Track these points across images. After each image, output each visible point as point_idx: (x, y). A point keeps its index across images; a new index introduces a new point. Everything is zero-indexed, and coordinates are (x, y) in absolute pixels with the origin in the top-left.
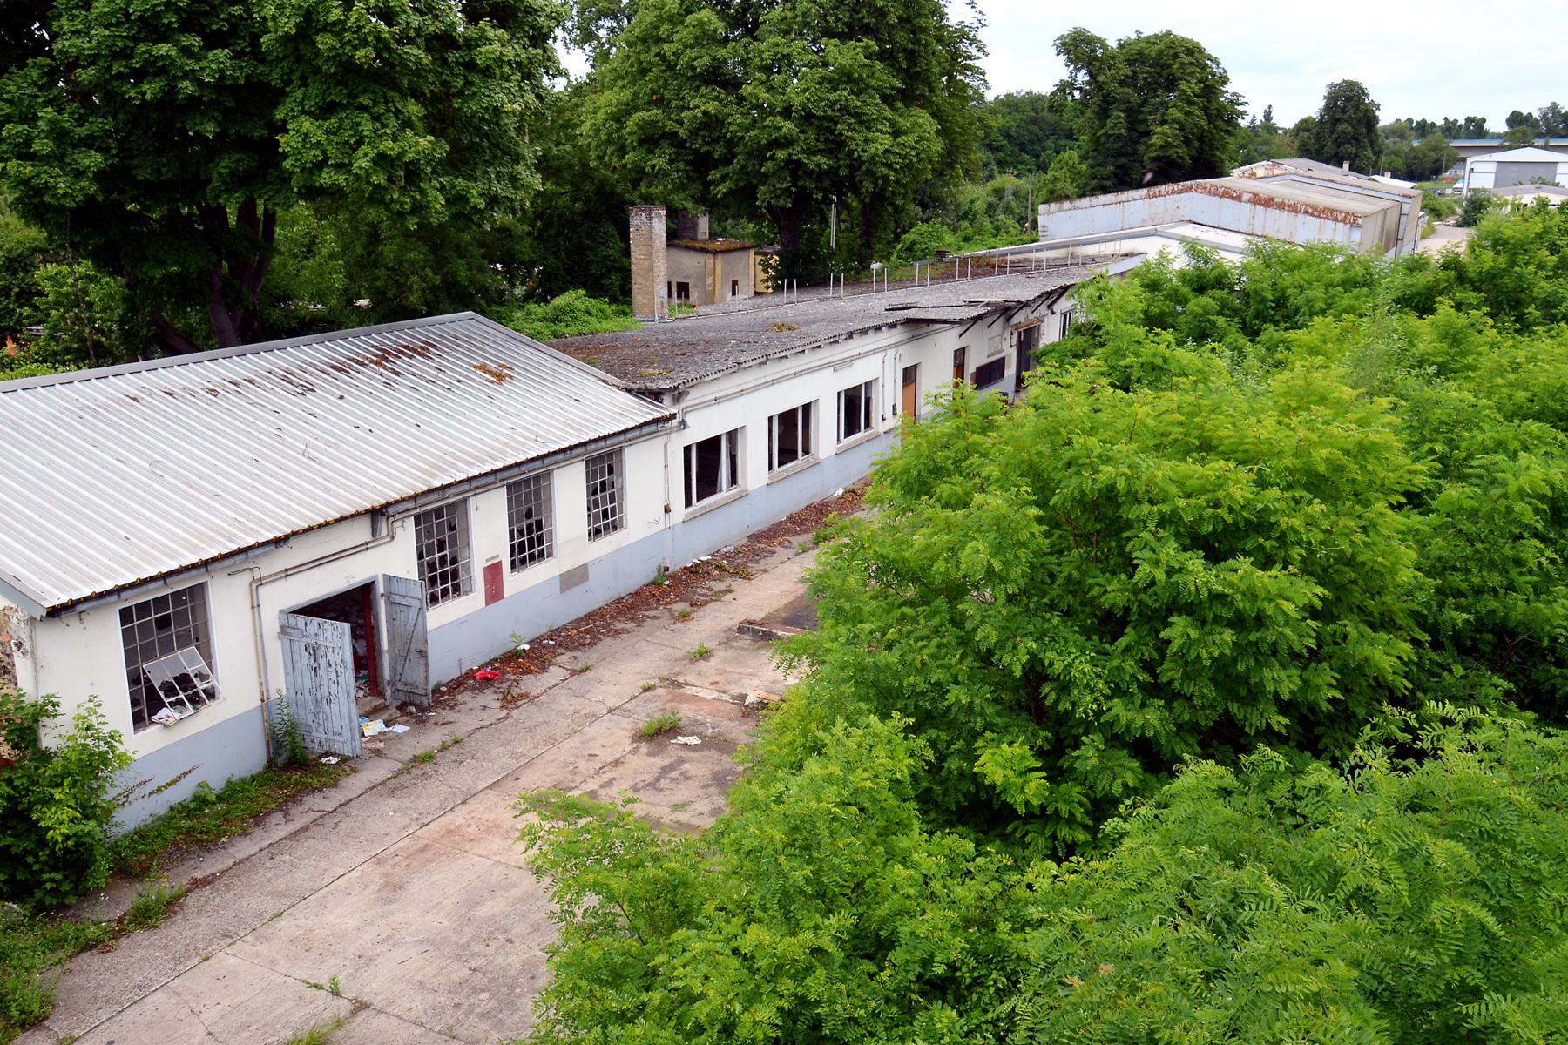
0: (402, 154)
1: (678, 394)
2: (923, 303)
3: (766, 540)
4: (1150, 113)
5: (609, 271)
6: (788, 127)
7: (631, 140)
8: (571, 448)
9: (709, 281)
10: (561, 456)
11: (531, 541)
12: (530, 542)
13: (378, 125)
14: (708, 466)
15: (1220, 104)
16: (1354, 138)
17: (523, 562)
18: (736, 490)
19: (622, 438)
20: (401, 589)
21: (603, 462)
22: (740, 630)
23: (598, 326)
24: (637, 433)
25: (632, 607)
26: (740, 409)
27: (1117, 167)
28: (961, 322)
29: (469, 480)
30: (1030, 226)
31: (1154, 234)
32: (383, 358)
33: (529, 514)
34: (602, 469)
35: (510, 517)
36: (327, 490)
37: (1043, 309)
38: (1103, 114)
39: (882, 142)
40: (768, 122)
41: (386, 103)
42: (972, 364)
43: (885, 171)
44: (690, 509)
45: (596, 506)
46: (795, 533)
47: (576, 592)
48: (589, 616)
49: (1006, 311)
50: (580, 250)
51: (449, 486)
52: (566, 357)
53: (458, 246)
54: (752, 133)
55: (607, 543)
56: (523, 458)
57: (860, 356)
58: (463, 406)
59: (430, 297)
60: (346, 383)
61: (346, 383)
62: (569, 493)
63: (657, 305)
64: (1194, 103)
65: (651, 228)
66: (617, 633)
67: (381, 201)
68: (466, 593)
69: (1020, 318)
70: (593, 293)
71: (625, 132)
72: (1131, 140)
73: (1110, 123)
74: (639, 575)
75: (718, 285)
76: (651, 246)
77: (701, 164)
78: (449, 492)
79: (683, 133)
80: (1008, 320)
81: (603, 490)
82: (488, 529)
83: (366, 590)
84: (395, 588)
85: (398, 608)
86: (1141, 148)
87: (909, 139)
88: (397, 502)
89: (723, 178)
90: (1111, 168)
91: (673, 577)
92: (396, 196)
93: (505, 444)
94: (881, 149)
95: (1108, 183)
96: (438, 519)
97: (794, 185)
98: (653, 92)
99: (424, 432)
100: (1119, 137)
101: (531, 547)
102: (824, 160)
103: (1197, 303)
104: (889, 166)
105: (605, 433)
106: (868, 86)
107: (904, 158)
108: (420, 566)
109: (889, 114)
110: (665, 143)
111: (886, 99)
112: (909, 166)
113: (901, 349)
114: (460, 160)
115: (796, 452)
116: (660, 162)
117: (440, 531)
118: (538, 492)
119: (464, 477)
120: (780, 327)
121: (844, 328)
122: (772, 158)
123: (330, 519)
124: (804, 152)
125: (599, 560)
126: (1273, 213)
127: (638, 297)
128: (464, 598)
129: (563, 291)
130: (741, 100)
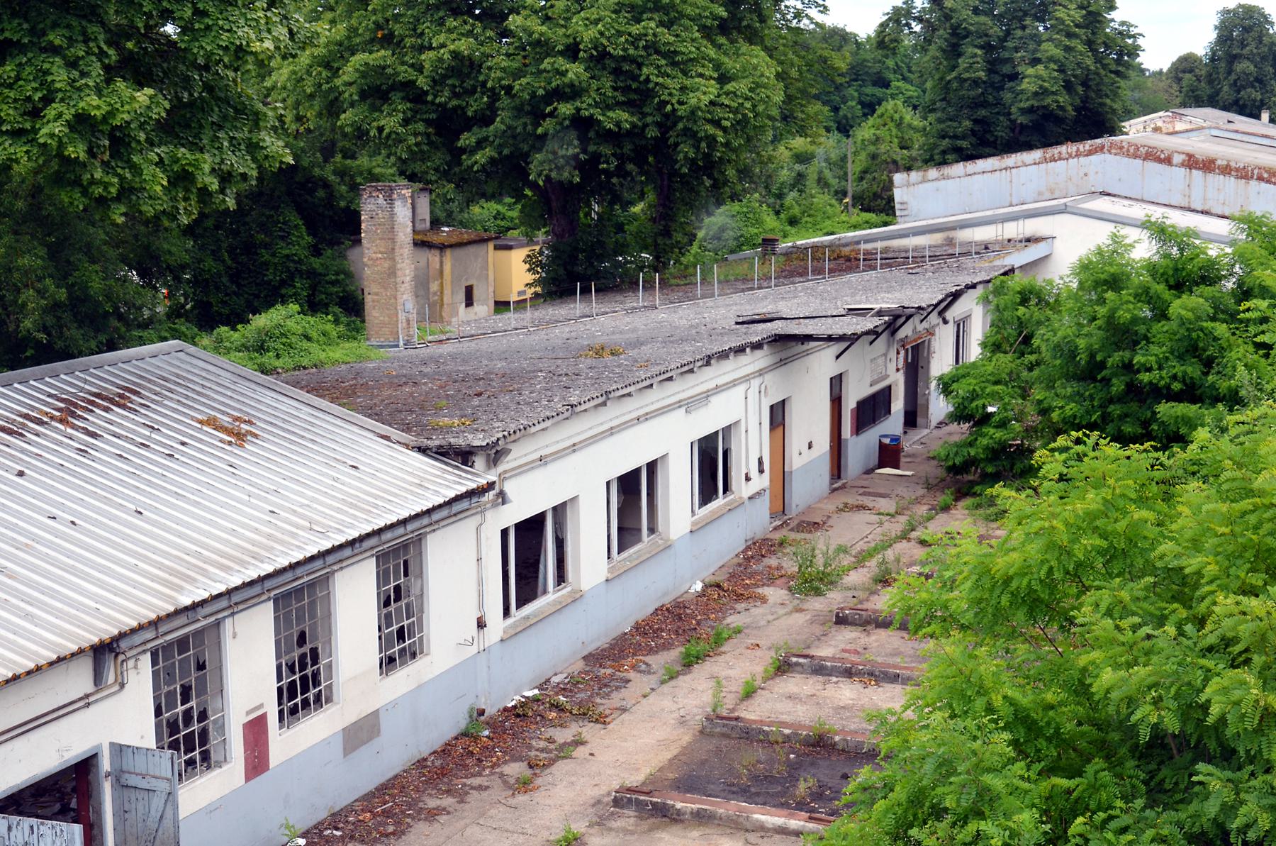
0: (112, 113)
1: (495, 454)
2: (785, 308)
3: (615, 658)
4: (1017, 49)
5: (292, 277)
6: (575, 71)
7: (351, 93)
8: (361, 539)
9: (434, 287)
10: (348, 552)
11: (304, 679)
12: (302, 685)
13: (76, 74)
14: (531, 553)
15: (1106, 35)
16: (1257, 80)
17: (294, 711)
18: (565, 590)
19: (425, 521)
20: (140, 764)
21: (397, 555)
22: (617, 802)
23: (323, 356)
24: (444, 513)
25: (443, 773)
26: (565, 474)
27: (976, 121)
28: (842, 338)
29: (229, 592)
30: (879, 204)
31: (1063, 210)
32: (69, 412)
33: (302, 639)
34: (397, 566)
35: (278, 643)
36: (28, 616)
37: (934, 318)
38: (953, 51)
39: (704, 92)
40: (546, 64)
41: (86, 42)
42: (853, 396)
43: (711, 129)
44: (510, 621)
45: (389, 625)
46: (651, 651)
47: (364, 753)
48: (383, 789)
49: (895, 321)
50: (250, 248)
51: (203, 603)
52: (323, 403)
53: (89, 246)
54: (524, 81)
55: (406, 678)
56: (299, 556)
57: (718, 389)
58: (196, 481)
59: (50, 320)
60: (23, 451)
61: (23, 451)
62: (355, 600)
63: (402, 325)
64: (1076, 36)
65: (392, 215)
66: (432, 815)
67: (77, 183)
68: (219, 765)
69: (906, 331)
70: (313, 306)
71: (338, 82)
72: (992, 85)
73: (963, 63)
74: (445, 724)
75: (447, 292)
76: (393, 240)
77: (448, 126)
78: (202, 612)
79: (422, 82)
80: (893, 333)
81: (398, 599)
82: (249, 663)
83: (83, 770)
84: (128, 763)
85: (133, 794)
86: (1007, 96)
87: (741, 86)
88: (133, 631)
89: (480, 144)
90: (967, 124)
91: (491, 724)
92: (98, 174)
93: (269, 536)
94: (705, 99)
95: (964, 144)
96: (181, 652)
97: (584, 151)
98: (378, 26)
99: (148, 521)
100: (976, 83)
101: (305, 689)
102: (625, 116)
103: (1181, 306)
104: (717, 123)
105: (405, 514)
106: (682, 15)
107: (736, 111)
108: (158, 726)
109: (712, 53)
110: (396, 96)
111: (706, 32)
112: (742, 123)
113: (768, 377)
114: (179, 125)
115: (640, 530)
116: (390, 122)
117: (185, 673)
118: (312, 604)
119: (222, 588)
120: (599, 352)
121: (689, 352)
122: (551, 115)
123: (42, 662)
124: (597, 105)
125: (394, 704)
126: (1216, 180)
127: (373, 312)
128: (215, 773)
129: (269, 304)
130: (505, 33)
